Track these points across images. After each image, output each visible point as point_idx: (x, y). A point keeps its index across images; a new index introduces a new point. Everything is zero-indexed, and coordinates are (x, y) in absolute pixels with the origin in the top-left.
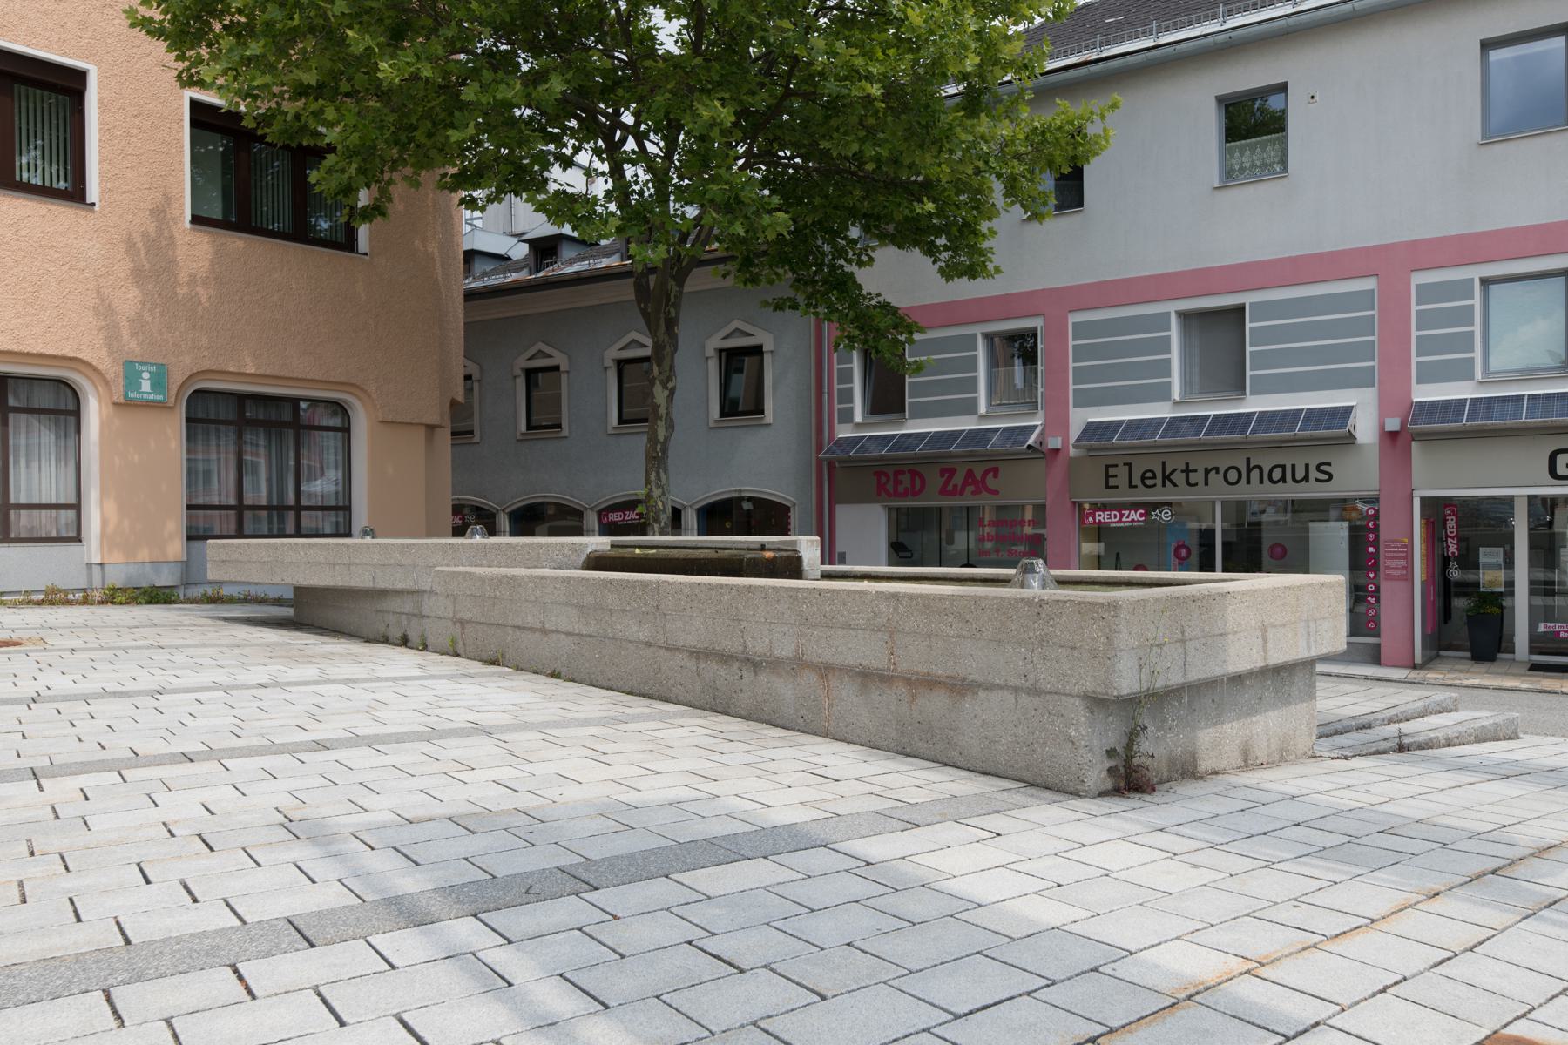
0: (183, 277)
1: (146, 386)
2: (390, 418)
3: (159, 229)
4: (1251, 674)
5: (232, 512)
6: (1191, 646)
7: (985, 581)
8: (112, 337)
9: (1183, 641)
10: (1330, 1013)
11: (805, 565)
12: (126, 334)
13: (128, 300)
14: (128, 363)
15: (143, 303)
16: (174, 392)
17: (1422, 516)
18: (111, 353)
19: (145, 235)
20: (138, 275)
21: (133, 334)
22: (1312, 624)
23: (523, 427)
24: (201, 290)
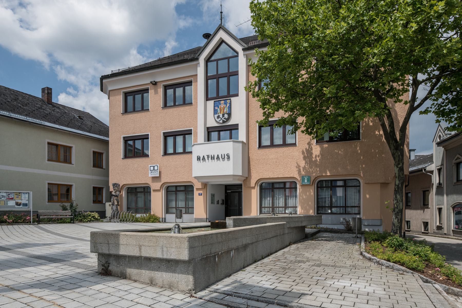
0: (314, 156)
1: (306, 181)
2: (367, 182)
3: (309, 147)
4: (155, 259)
5: (334, 205)
6: (111, 245)
7: (456, 239)
8: (299, 171)
9: (108, 244)
10: (36, 303)
11: (227, 224)
12: (302, 170)
13: (302, 164)
14: (303, 177)
15: (305, 163)
16: (312, 181)
17: (222, 222)
18: (299, 175)
19: (306, 149)
20: (305, 158)
21: (303, 171)
22: (165, 249)
23: (455, 181)
24: (317, 158)
